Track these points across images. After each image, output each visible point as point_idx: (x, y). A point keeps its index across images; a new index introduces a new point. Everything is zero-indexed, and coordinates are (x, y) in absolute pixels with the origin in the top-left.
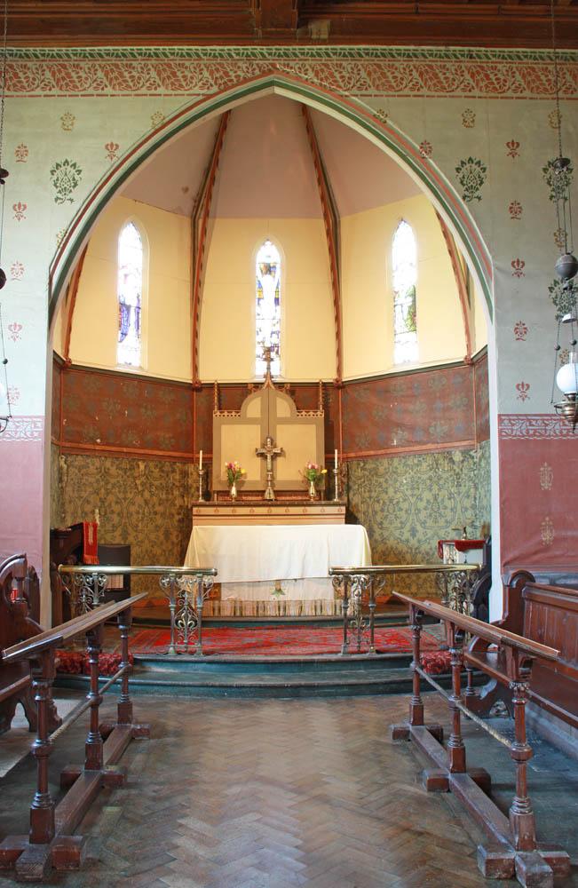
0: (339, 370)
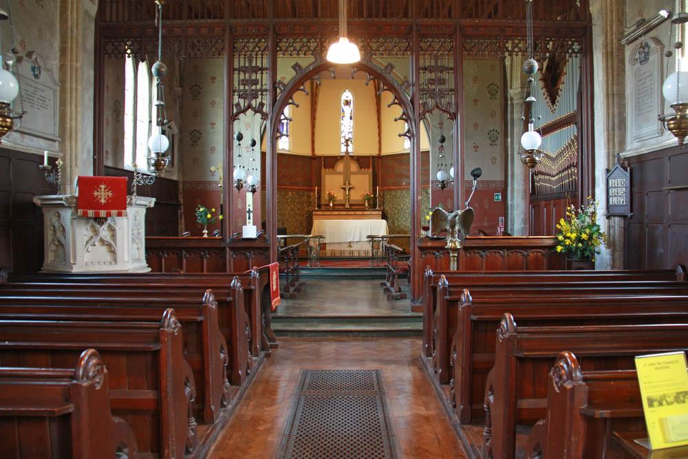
0: (380, 150)
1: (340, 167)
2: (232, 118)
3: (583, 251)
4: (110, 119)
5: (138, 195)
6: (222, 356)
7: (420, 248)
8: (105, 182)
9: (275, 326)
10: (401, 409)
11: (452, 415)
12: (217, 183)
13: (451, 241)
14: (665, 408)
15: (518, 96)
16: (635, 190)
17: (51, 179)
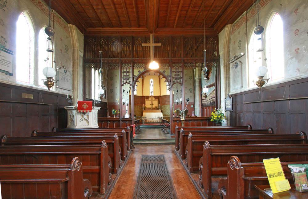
0: (160, 94)
1: (150, 99)
2: (122, 85)
3: (219, 121)
4: (88, 86)
6: (120, 152)
7: (173, 120)
8: (86, 102)
9: (134, 142)
10: (171, 168)
11: (187, 170)
12: (118, 103)
13: (182, 118)
14: (275, 178)
15: (198, 79)
16: (233, 104)
17: (69, 102)
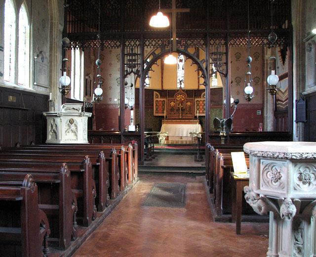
2: (124, 76)
5: (85, 111)
7: (209, 136)
